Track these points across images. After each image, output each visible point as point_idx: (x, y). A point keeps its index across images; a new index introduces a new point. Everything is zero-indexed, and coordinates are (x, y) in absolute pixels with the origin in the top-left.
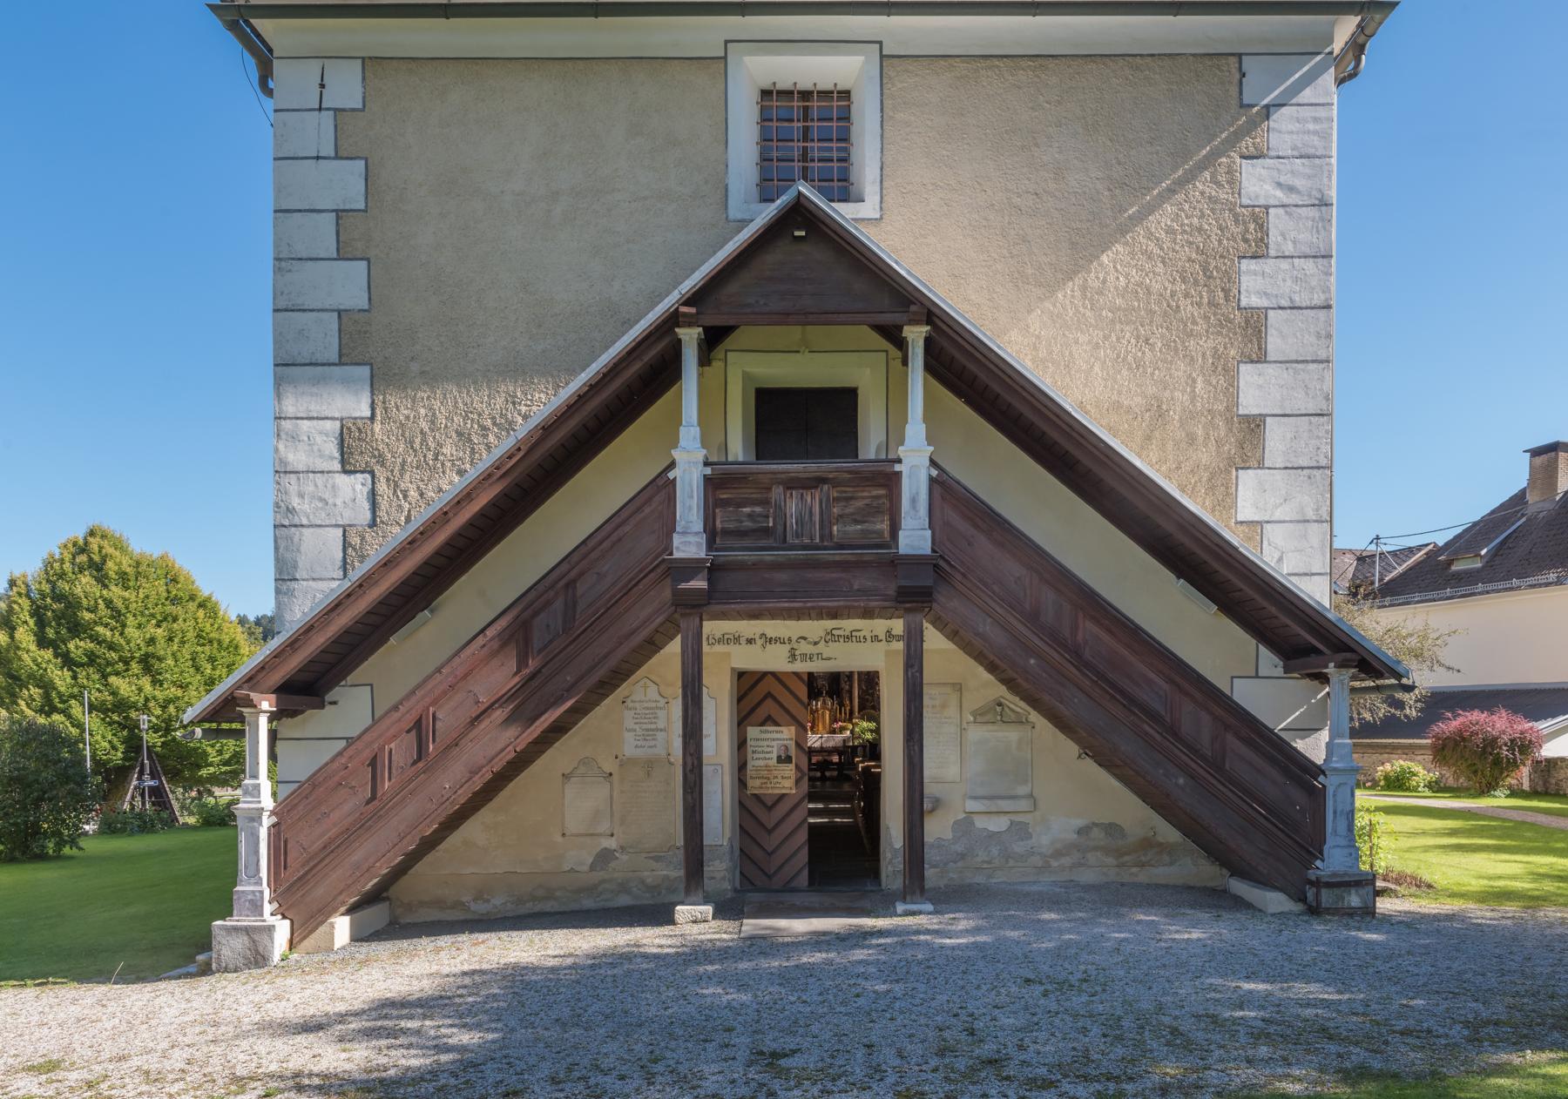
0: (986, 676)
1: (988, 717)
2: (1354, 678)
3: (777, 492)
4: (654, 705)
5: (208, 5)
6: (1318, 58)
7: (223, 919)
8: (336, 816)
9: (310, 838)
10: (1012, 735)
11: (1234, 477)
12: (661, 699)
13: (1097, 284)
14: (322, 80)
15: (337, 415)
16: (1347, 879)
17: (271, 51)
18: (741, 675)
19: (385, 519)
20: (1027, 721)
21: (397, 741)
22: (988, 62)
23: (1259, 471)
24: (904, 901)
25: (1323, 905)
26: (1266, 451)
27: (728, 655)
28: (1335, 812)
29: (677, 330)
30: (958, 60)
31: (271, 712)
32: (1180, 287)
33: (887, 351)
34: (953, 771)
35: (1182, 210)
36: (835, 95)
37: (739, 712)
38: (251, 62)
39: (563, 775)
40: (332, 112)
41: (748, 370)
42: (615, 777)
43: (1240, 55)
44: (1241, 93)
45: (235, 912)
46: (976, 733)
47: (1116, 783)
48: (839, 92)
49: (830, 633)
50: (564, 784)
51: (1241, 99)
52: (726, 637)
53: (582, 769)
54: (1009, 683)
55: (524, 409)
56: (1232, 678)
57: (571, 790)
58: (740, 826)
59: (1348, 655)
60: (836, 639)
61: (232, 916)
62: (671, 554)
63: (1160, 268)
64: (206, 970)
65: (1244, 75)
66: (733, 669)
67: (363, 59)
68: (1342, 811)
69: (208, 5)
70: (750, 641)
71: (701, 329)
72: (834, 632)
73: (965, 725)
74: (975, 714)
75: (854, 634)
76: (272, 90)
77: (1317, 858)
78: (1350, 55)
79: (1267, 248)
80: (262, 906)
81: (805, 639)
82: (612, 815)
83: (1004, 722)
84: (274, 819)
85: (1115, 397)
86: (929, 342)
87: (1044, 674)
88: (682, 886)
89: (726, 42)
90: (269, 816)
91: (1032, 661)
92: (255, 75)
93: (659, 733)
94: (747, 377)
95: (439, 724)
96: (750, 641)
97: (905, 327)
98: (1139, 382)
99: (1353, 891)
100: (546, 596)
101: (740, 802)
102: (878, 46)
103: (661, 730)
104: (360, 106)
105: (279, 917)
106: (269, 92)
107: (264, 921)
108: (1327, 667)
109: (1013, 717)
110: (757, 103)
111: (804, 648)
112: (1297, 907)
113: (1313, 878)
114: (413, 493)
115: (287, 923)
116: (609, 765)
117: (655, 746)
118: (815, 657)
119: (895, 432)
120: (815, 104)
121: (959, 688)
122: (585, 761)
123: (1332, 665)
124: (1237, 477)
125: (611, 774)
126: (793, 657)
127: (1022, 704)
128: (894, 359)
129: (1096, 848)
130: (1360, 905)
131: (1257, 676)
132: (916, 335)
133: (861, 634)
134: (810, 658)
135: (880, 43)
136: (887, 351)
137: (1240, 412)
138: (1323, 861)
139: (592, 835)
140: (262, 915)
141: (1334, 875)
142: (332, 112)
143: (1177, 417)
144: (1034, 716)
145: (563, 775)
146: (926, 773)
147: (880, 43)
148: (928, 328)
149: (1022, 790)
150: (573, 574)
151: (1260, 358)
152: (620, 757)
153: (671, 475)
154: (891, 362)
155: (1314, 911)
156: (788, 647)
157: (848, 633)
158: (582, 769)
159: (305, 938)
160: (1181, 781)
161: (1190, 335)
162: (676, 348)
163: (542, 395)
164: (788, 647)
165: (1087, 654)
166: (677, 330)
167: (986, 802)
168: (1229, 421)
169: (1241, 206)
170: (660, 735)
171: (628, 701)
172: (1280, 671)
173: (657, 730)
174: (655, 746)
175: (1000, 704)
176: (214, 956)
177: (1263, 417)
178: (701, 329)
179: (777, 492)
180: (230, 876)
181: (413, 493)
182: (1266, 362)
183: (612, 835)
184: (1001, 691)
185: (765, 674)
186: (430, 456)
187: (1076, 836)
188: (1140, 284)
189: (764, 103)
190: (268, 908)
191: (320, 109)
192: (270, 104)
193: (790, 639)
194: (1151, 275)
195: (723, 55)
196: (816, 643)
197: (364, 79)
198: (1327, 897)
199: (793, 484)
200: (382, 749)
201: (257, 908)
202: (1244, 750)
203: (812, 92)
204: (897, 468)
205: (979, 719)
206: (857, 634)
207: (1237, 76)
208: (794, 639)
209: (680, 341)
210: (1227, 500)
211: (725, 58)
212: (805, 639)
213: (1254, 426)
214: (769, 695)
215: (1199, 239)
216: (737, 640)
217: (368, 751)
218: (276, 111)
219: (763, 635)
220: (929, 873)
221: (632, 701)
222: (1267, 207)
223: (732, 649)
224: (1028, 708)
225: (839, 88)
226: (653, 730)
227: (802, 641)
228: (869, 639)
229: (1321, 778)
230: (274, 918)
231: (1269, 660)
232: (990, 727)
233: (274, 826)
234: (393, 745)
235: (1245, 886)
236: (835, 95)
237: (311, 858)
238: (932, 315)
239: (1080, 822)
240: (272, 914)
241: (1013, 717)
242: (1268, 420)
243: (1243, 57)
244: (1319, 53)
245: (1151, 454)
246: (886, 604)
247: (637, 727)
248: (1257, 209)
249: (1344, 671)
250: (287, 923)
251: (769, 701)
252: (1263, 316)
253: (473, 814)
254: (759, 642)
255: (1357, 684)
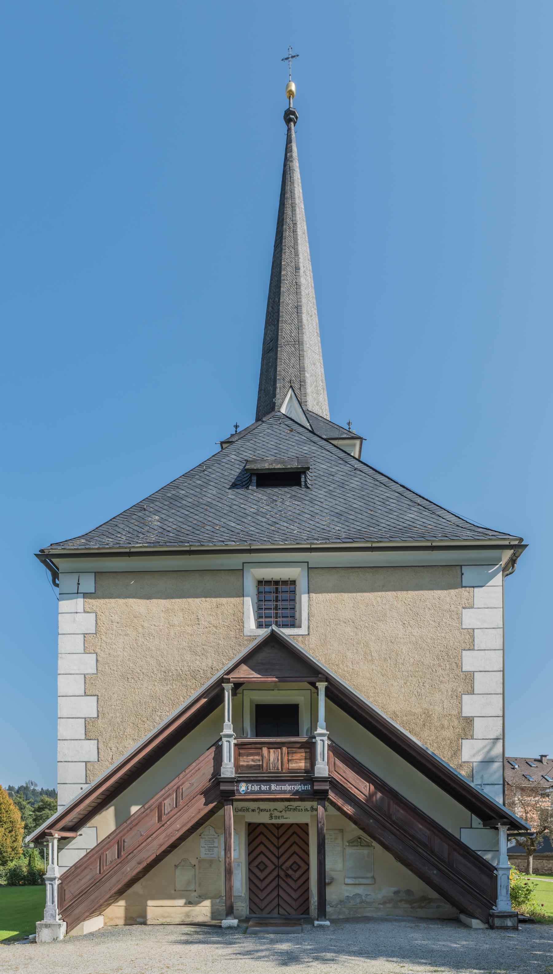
0: (354, 826)
1: (355, 844)
2: (508, 830)
3: (265, 750)
4: (213, 837)
5: (35, 554)
6: (498, 566)
7: (40, 921)
8: (84, 881)
9: (73, 889)
10: (365, 851)
11: (460, 743)
12: (216, 834)
13: (401, 661)
14: (79, 581)
15: (83, 717)
16: (506, 914)
17: (58, 569)
18: (249, 824)
19: (103, 759)
20: (372, 846)
21: (109, 851)
22: (353, 570)
23: (471, 740)
24: (318, 920)
25: (496, 925)
26: (474, 732)
27: (243, 816)
28: (501, 886)
29: (222, 684)
30: (340, 569)
31: (59, 838)
32: (436, 662)
33: (311, 690)
34: (339, 866)
35: (437, 630)
36: (289, 582)
37: (249, 840)
38: (49, 573)
39: (175, 865)
40: (82, 594)
41: (252, 697)
42: (197, 867)
43: (461, 566)
44: (462, 582)
45: (45, 919)
46: (349, 851)
47: (410, 873)
48: (290, 581)
49: (287, 807)
50: (175, 869)
51: (462, 584)
52: (243, 808)
53: (183, 863)
54: (363, 829)
55: (159, 714)
56: (461, 828)
57: (178, 872)
58: (249, 888)
59: (505, 820)
60: (290, 810)
61: (43, 920)
62: (220, 776)
63: (428, 654)
64: (34, 942)
65: (462, 574)
66: (246, 822)
67: (95, 573)
68: (504, 886)
69: (35, 554)
70: (253, 810)
71: (232, 684)
72: (289, 807)
73: (344, 847)
74: (349, 842)
75: (297, 808)
76: (58, 584)
77: (494, 905)
78: (510, 564)
79: (474, 646)
80: (55, 916)
81: (276, 810)
82: (195, 883)
83: (362, 846)
84: (60, 881)
85: (409, 709)
86: (327, 688)
87: (376, 827)
88: (225, 913)
89: (243, 563)
90: (58, 880)
91: (371, 821)
92: (50, 578)
93: (215, 849)
94: (251, 701)
95: (125, 844)
96: (253, 810)
97: (317, 683)
98: (419, 702)
99: (508, 919)
100: (169, 792)
101: (249, 878)
102: (307, 564)
103: (216, 847)
104: (94, 592)
105: (62, 921)
106: (57, 585)
107: (57, 922)
108: (498, 825)
109: (365, 844)
110: (256, 587)
111: (276, 814)
112: (487, 926)
113: (491, 914)
114: (114, 749)
115: (65, 923)
116: (194, 862)
117: (213, 854)
118: (281, 818)
119: (314, 725)
120: (280, 587)
121: (342, 831)
122: (185, 860)
123: (499, 824)
124: (462, 743)
125: (195, 865)
126: (271, 817)
127: (369, 838)
128: (314, 693)
129: (401, 901)
130: (512, 925)
131: (471, 828)
132: (322, 686)
133: (301, 808)
134: (279, 818)
135: (308, 562)
136: (311, 690)
137: (463, 716)
138: (496, 906)
139: (187, 891)
140: (55, 920)
141: (500, 912)
142: (82, 594)
143: (436, 717)
144: (374, 843)
145: (175, 865)
146: (327, 867)
147: (308, 562)
148: (327, 683)
149: (370, 875)
150: (180, 783)
151: (472, 692)
152: (199, 858)
153: (220, 743)
154: (313, 694)
155: (492, 927)
156: (269, 813)
157: (294, 807)
158: (183, 863)
159: (72, 929)
160: (435, 872)
161: (441, 682)
162: (223, 690)
163: (167, 708)
164: (269, 813)
165: (394, 818)
166: (222, 684)
167: (354, 880)
168: (458, 718)
169: (462, 629)
170: (216, 850)
171: (202, 835)
172: (481, 826)
173: (214, 847)
174: (213, 854)
175: (360, 838)
176: (37, 935)
177: (473, 717)
178: (232, 684)
179: (265, 750)
180: (43, 904)
181: (114, 749)
182: (474, 694)
183: (195, 891)
184: (361, 833)
185: (259, 824)
186: (121, 733)
187: (393, 895)
188: (419, 661)
189: (259, 603)
190: (58, 917)
191: (78, 593)
192: (57, 590)
193: (270, 810)
194: (424, 657)
195: (242, 568)
196: (281, 812)
197: (95, 581)
198: (497, 922)
199: (271, 746)
200: (103, 853)
201: (54, 917)
202: (460, 858)
203: (280, 581)
204: (314, 740)
205: (351, 844)
206: (299, 808)
207: (460, 574)
208: (272, 810)
209: (224, 688)
210: (457, 752)
211: (243, 570)
212: (276, 810)
213: (469, 721)
214: (261, 833)
215: (445, 642)
216: (248, 810)
217: (97, 854)
218: (60, 594)
219: (259, 808)
220: (329, 909)
221: (204, 835)
222: (474, 629)
223: (245, 813)
224: (372, 840)
225: (290, 580)
226: (212, 847)
227: (275, 811)
228: (303, 810)
229: (495, 872)
230: (60, 921)
231: (476, 821)
232: (356, 848)
233: (60, 884)
234: (107, 852)
235: (465, 917)
236: (289, 582)
237: (75, 897)
238: (327, 678)
239: (395, 889)
240: (59, 920)
241: (365, 844)
242: (475, 718)
243: (463, 567)
244: (497, 565)
245: (425, 733)
246: (310, 796)
247: (206, 846)
248: (469, 630)
249: (504, 827)
250: (65, 923)
251: (262, 836)
252: (472, 675)
253: (138, 881)
254: (257, 811)
255: (512, 832)
